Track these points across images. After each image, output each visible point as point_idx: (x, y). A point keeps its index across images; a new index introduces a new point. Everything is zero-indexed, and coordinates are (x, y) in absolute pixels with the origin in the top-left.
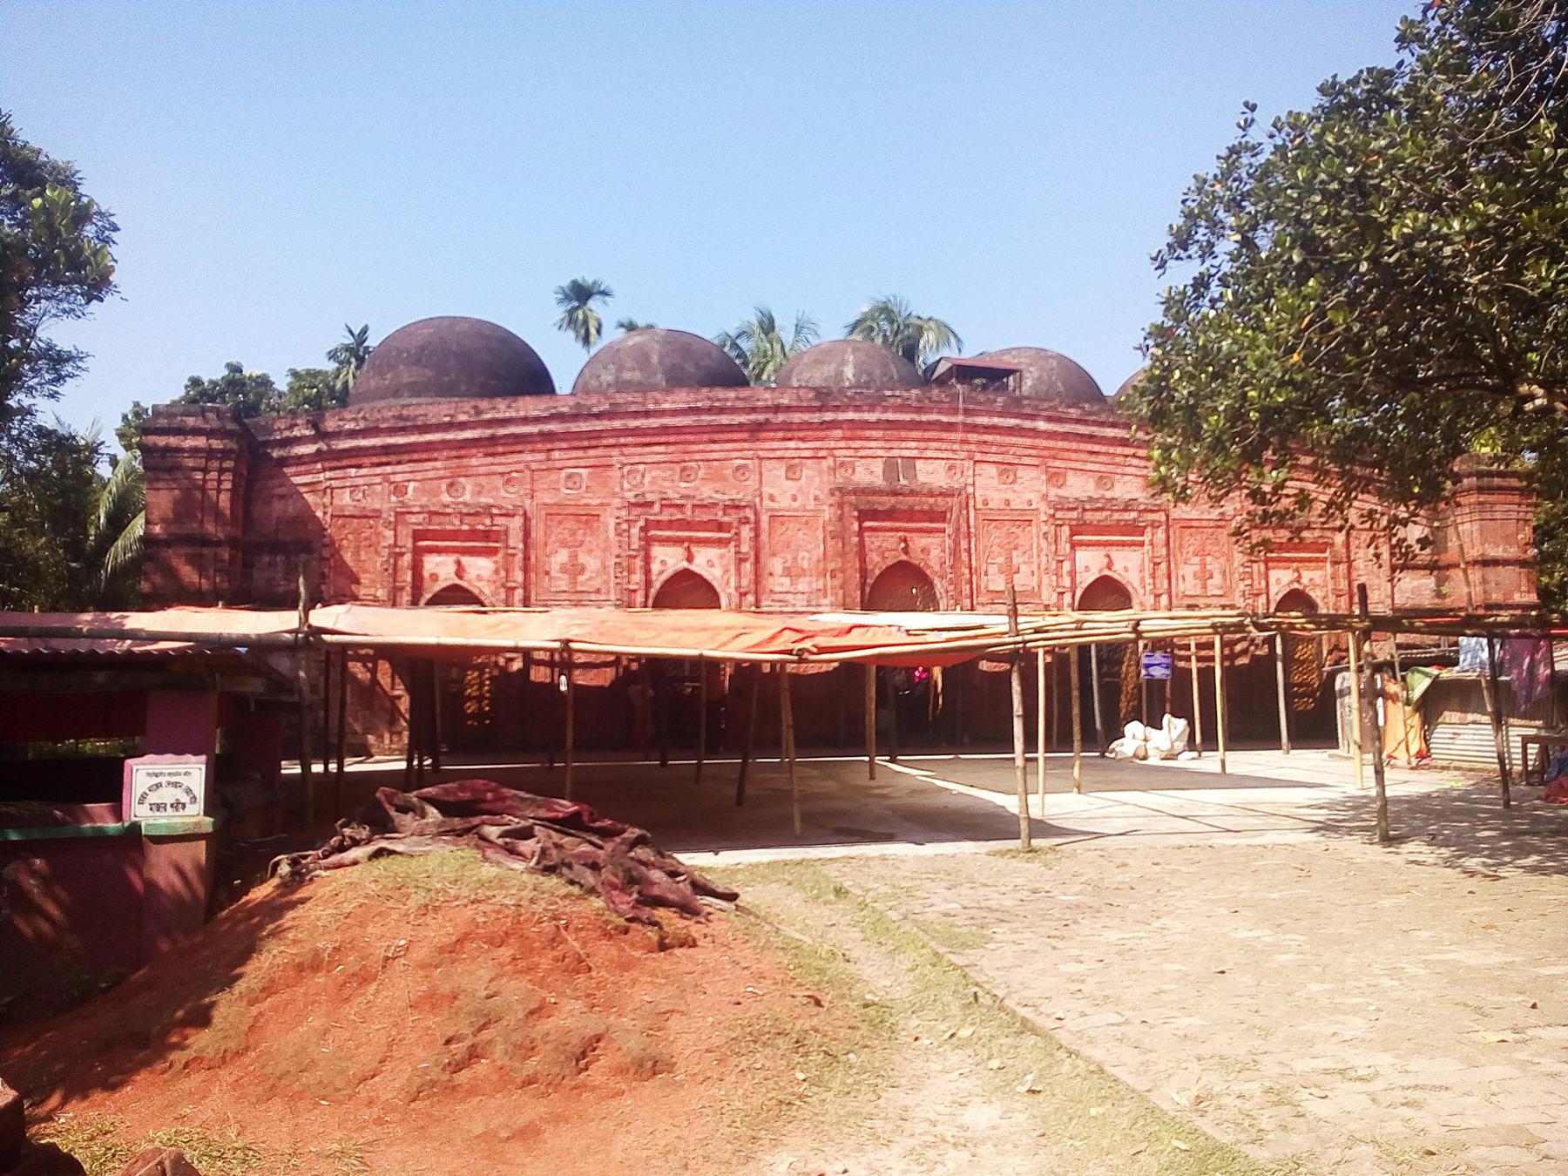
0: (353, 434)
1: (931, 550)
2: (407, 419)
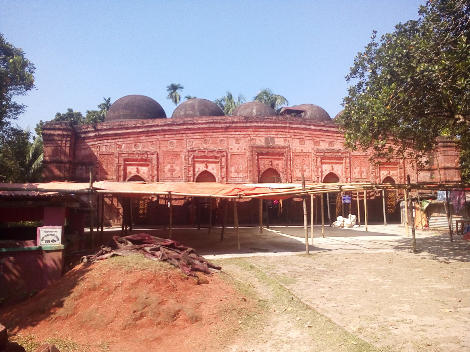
0: (106, 130)
1: (279, 164)
2: (122, 125)
